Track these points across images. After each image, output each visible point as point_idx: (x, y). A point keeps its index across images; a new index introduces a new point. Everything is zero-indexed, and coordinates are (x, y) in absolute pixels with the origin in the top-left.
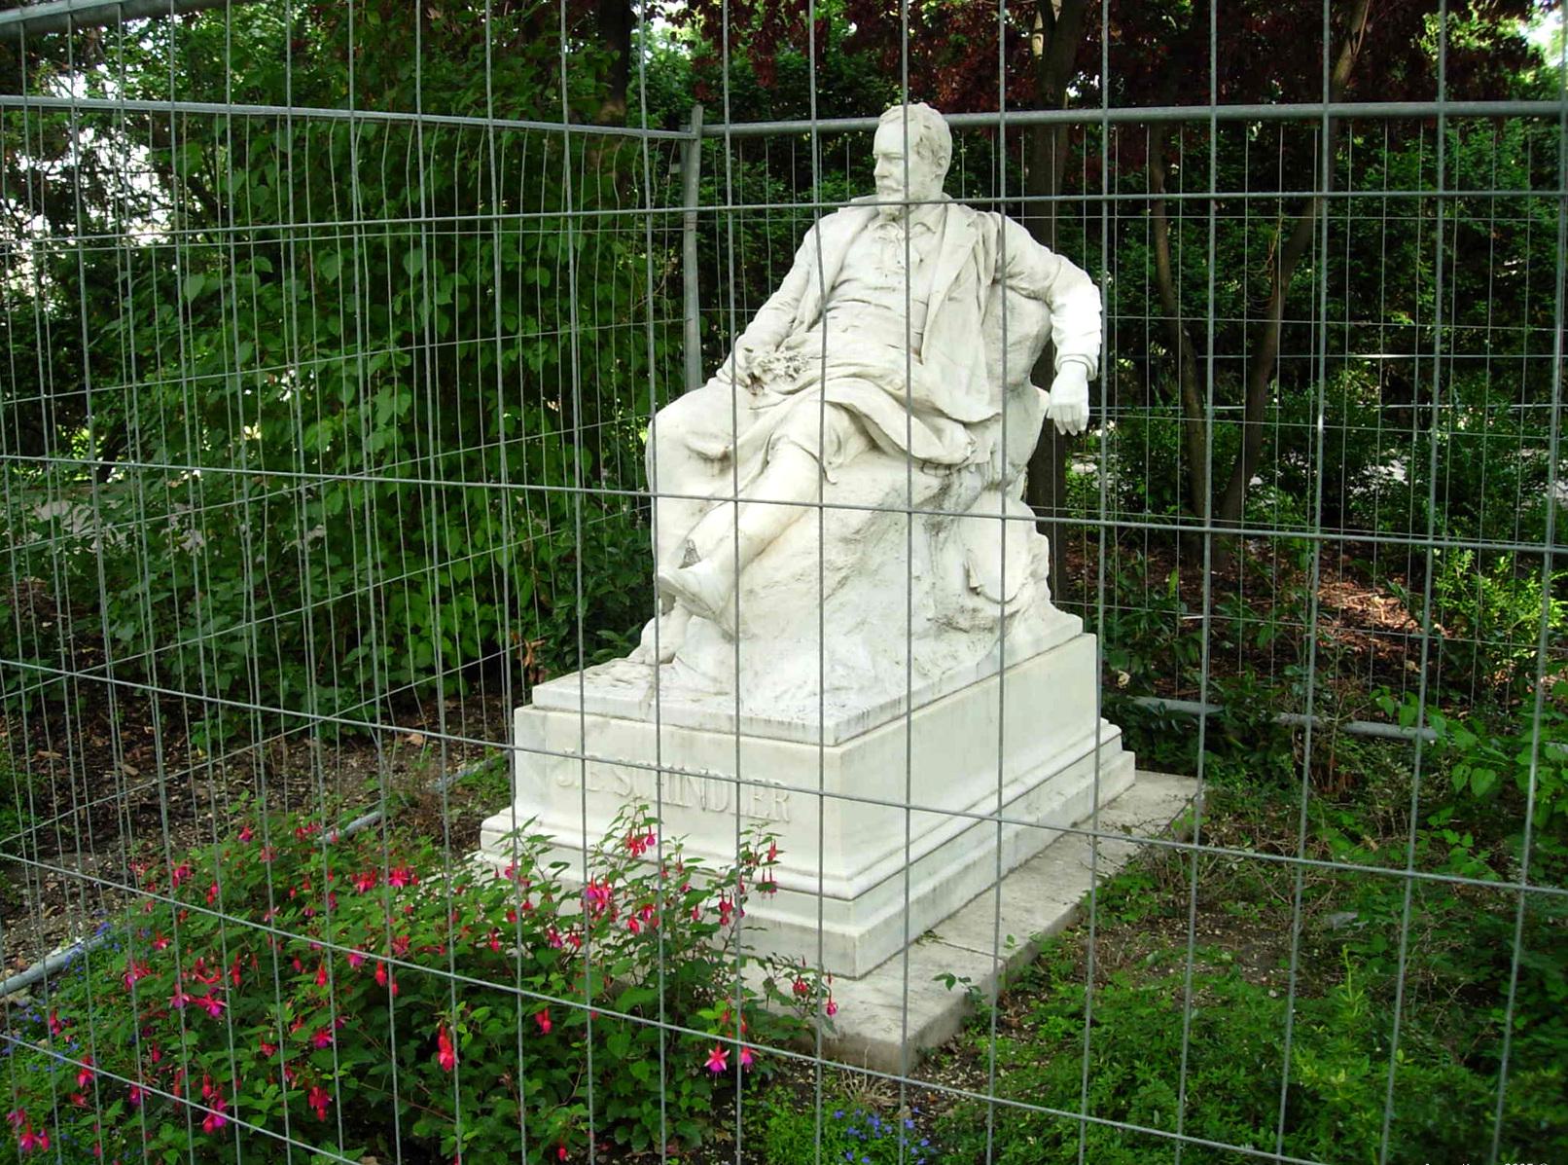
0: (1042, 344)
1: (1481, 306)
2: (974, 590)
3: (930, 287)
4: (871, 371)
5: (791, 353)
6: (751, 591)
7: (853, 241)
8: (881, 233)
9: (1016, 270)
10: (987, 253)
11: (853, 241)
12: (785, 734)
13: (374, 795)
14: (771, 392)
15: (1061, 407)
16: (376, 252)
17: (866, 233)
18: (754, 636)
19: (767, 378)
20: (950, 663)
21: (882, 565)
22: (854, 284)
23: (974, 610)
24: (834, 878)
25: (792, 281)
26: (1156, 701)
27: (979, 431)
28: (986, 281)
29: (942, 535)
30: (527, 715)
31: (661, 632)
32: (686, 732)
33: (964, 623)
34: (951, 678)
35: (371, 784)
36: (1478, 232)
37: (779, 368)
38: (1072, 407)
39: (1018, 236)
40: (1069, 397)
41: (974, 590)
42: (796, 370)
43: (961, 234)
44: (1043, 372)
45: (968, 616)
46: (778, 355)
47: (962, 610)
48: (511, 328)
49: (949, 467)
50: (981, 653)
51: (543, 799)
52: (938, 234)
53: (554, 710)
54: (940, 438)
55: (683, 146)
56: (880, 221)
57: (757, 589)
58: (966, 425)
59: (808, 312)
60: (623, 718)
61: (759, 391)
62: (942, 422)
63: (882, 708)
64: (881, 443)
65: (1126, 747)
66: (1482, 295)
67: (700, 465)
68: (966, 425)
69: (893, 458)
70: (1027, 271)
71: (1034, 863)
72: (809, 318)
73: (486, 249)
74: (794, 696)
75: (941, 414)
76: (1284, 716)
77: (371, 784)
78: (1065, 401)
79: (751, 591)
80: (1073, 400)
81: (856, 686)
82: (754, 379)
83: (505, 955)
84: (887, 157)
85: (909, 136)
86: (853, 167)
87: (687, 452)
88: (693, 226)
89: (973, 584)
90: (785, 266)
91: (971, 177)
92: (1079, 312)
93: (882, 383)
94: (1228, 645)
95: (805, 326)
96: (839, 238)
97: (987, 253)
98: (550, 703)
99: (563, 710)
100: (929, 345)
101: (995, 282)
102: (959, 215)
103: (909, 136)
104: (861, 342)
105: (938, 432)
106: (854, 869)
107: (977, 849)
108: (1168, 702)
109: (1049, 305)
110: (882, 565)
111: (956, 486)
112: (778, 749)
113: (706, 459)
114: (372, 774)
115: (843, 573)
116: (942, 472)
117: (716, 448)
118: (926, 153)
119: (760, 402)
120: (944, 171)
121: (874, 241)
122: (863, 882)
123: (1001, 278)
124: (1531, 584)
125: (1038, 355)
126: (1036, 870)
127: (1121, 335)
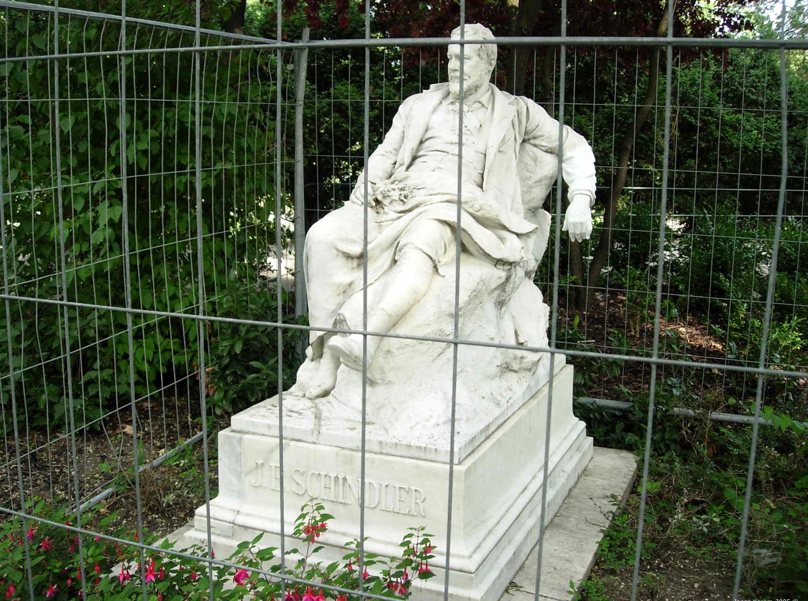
1: (691, 162)
3: (487, 145)
5: (401, 185)
6: (388, 352)
7: (435, 110)
9: (539, 134)
10: (520, 122)
11: (435, 110)
12: (422, 455)
13: (108, 477)
14: (390, 211)
15: (574, 224)
16: (97, 115)
17: (442, 107)
18: (390, 382)
19: (386, 202)
20: (510, 394)
21: (474, 331)
22: (436, 140)
23: (522, 358)
24: (459, 556)
25: (391, 137)
26: (591, 400)
27: (524, 238)
28: (519, 141)
29: (503, 309)
30: (228, 437)
31: (311, 374)
32: (347, 452)
33: (515, 366)
34: (512, 405)
35: (105, 467)
36: (691, 123)
37: (395, 195)
38: (582, 224)
39: (537, 112)
40: (581, 218)
42: (406, 197)
43: (508, 112)
44: (556, 198)
45: (518, 362)
46: (393, 186)
47: (515, 358)
48: (184, 162)
49: (511, 264)
50: (525, 385)
51: (240, 495)
52: (490, 107)
53: (248, 433)
55: (296, 52)
56: (450, 99)
57: (392, 350)
58: (518, 235)
59: (405, 156)
60: (298, 440)
61: (380, 210)
62: (505, 234)
63: (481, 432)
65: (588, 435)
66: (693, 156)
67: (342, 260)
68: (518, 235)
69: (479, 258)
70: (546, 134)
71: (556, 520)
72: (407, 161)
73: (169, 115)
74: (424, 426)
75: (505, 228)
76: (676, 409)
77: (105, 467)
78: (577, 220)
79: (388, 352)
80: (583, 220)
81: (464, 418)
82: (377, 201)
83: (193, 568)
85: (472, 47)
87: (335, 252)
88: (302, 103)
89: (521, 341)
90: (389, 124)
91: (512, 75)
92: (581, 165)
95: (405, 167)
96: (419, 111)
97: (520, 122)
98: (244, 427)
99: (254, 433)
100: (487, 184)
101: (524, 141)
102: (502, 97)
103: (472, 47)
104: (434, 178)
105: (502, 239)
106: (472, 549)
107: (531, 522)
108: (597, 400)
110: (474, 331)
111: (513, 276)
112: (418, 467)
113: (348, 257)
114: (103, 458)
116: (507, 267)
117: (357, 250)
118: (484, 56)
119: (383, 217)
120: (492, 69)
121: (448, 112)
122: (478, 557)
124: (785, 325)
126: (559, 526)
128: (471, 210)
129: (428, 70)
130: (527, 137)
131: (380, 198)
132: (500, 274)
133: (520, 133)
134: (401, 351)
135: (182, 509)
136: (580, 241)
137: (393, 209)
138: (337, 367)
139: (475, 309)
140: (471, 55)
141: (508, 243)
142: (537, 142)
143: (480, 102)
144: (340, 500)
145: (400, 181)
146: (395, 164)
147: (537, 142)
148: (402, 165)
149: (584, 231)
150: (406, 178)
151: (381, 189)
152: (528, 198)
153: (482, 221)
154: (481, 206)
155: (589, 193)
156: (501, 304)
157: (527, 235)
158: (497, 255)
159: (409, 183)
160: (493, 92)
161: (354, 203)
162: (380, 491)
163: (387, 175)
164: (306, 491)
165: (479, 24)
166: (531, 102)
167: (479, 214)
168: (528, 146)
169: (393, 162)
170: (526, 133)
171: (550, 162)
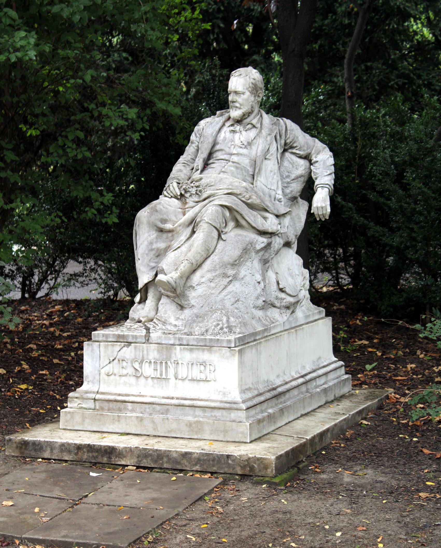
0: (306, 179)
2: (281, 290)
4: (235, 191)
5: (197, 184)
8: (232, 128)
9: (295, 145)
19: (187, 195)
21: (245, 276)
25: (190, 150)
27: (282, 218)
28: (280, 151)
33: (278, 305)
37: (193, 191)
40: (322, 201)
41: (281, 290)
42: (200, 191)
44: (308, 191)
45: (279, 301)
46: (192, 185)
54: (266, 221)
59: (199, 163)
62: (267, 215)
64: (243, 223)
72: (200, 168)
84: (236, 93)
85: (243, 82)
86: (218, 101)
89: (281, 286)
91: (280, 104)
92: (324, 164)
93: (240, 197)
94: (359, 85)
95: (199, 171)
101: (285, 150)
102: (267, 119)
105: (265, 218)
109: (310, 161)
111: (273, 243)
115: (231, 278)
123: (287, 148)
125: (304, 184)
127: (340, 172)
128: (243, 199)
129: (218, 101)
130: (286, 148)
131: (183, 192)
132: (262, 241)
133: (280, 145)
134: (198, 287)
135: (267, 67)
136: (323, 220)
137: (193, 200)
138: (159, 300)
139: (246, 261)
140: (244, 91)
141: (269, 221)
142: (294, 151)
143: (252, 124)
144: (164, 376)
145: (196, 182)
146: (193, 169)
147: (294, 151)
148: (197, 170)
149: (324, 212)
150: (201, 179)
151: (184, 187)
152: (288, 191)
153: (251, 206)
154: (250, 196)
155: (327, 186)
156: (265, 262)
157: (284, 215)
158: (261, 228)
159: (203, 182)
160: (261, 116)
161: (166, 196)
162: (188, 368)
163: (187, 177)
164: (142, 373)
165: (250, 68)
166: (289, 122)
167: (249, 201)
168: (287, 154)
169: (191, 168)
170: (286, 144)
171: (301, 167)
